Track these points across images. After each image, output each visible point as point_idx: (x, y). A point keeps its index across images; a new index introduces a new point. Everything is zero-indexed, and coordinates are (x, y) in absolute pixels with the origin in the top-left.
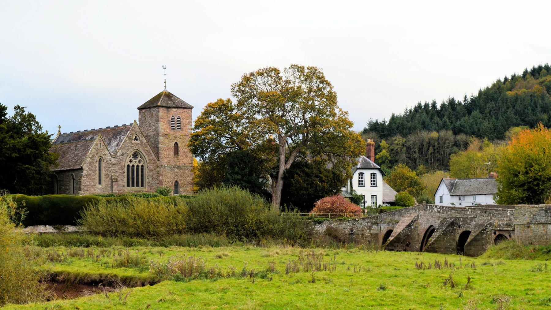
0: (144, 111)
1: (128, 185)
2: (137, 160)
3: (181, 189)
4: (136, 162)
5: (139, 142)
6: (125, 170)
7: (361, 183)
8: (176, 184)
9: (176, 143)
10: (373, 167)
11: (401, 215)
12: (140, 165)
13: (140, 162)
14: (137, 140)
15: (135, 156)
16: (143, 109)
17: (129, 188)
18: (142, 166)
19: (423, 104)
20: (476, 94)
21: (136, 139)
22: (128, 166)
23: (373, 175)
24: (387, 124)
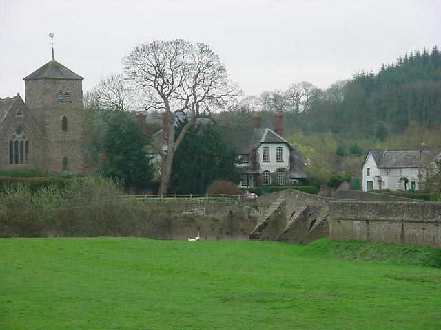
0: (30, 82)
1: (11, 163)
2: (21, 136)
3: (70, 166)
4: (19, 138)
5: (22, 116)
6: (8, 146)
7: (266, 159)
8: (65, 162)
9: (64, 117)
10: (279, 141)
11: (274, 200)
12: (25, 141)
13: (24, 137)
14: (20, 114)
15: (19, 132)
16: (30, 80)
17: (12, 166)
18: (27, 142)
19: (421, 53)
20: (376, 71)
21: (19, 113)
22: (11, 142)
23: (280, 149)
24: (429, 54)
